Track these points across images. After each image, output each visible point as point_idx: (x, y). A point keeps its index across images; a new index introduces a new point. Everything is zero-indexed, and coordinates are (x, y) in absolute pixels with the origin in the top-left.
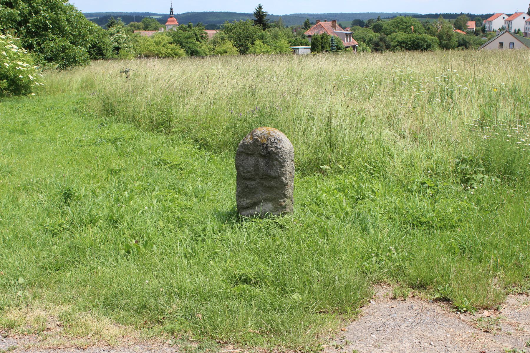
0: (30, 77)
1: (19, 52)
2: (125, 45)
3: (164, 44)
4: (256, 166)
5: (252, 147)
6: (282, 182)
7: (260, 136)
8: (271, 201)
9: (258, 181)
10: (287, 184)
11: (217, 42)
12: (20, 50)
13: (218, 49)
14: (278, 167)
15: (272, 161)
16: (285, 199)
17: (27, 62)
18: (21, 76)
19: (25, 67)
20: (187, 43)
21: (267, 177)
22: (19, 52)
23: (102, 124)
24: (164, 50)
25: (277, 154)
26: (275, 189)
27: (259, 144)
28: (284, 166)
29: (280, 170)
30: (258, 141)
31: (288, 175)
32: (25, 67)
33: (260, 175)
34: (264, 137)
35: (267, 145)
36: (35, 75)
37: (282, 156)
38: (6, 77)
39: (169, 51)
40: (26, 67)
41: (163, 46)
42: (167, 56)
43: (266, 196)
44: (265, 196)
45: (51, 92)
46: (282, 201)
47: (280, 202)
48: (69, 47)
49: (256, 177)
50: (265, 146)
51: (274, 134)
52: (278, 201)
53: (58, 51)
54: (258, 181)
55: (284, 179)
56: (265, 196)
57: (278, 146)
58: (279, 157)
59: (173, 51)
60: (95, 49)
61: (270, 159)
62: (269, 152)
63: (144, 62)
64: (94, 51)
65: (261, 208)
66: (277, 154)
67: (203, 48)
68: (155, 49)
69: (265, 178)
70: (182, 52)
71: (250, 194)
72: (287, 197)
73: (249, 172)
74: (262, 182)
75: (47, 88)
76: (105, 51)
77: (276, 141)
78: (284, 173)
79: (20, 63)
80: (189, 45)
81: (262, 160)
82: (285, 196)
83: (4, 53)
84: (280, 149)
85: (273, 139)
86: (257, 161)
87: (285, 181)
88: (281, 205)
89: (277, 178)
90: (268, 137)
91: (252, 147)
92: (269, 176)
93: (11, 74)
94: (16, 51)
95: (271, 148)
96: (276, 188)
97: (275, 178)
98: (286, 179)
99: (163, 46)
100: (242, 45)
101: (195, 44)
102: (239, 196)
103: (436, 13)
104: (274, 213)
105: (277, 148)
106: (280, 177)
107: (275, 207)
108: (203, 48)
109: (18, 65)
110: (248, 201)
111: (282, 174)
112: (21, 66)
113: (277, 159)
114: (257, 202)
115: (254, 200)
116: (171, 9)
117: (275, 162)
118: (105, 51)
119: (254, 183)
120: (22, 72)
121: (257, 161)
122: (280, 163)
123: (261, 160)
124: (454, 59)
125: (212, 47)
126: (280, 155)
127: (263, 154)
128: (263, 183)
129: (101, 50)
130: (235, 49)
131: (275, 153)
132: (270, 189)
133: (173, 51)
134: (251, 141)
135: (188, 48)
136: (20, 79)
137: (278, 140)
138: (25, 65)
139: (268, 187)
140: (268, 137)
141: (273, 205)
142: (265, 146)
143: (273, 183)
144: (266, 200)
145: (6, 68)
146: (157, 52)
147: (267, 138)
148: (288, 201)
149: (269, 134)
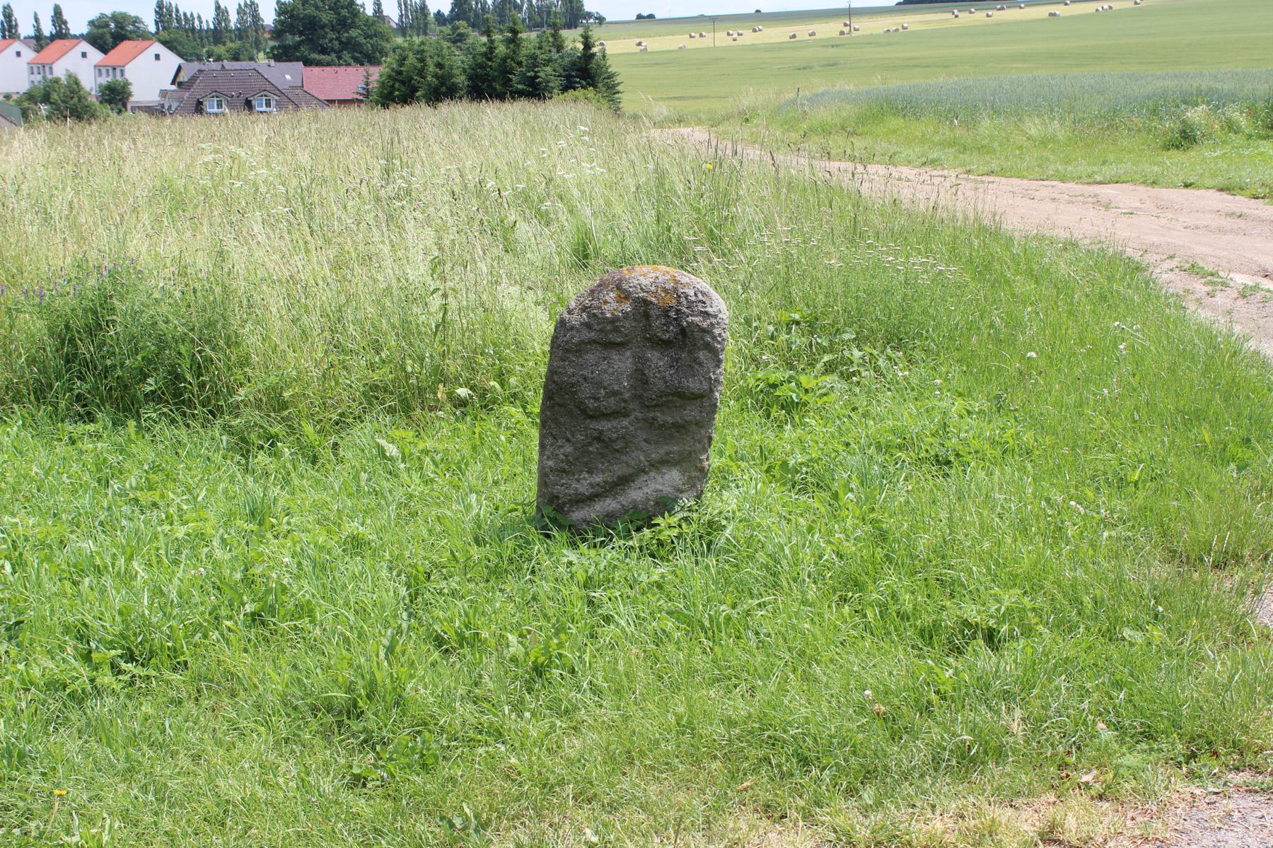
4: (641, 378)
7: (653, 289)
34: (665, 290)
35: (678, 312)
43: (662, 451)
44: (657, 453)
50: (672, 314)
56: (657, 453)
57: (709, 309)
58: (714, 338)
62: (683, 331)
73: (615, 394)
74: (651, 415)
77: (700, 297)
81: (657, 354)
84: (716, 317)
85: (692, 293)
95: (690, 319)
96: (697, 424)
103: (123, 10)
107: (690, 477)
110: (598, 478)
114: (631, 475)
115: (620, 470)
116: (37, 20)
119: (625, 422)
121: (640, 360)
123: (653, 356)
124: (498, 120)
126: (717, 331)
131: (704, 331)
134: (627, 307)
140: (675, 289)
141: (683, 472)
142: (672, 314)
149: (677, 282)
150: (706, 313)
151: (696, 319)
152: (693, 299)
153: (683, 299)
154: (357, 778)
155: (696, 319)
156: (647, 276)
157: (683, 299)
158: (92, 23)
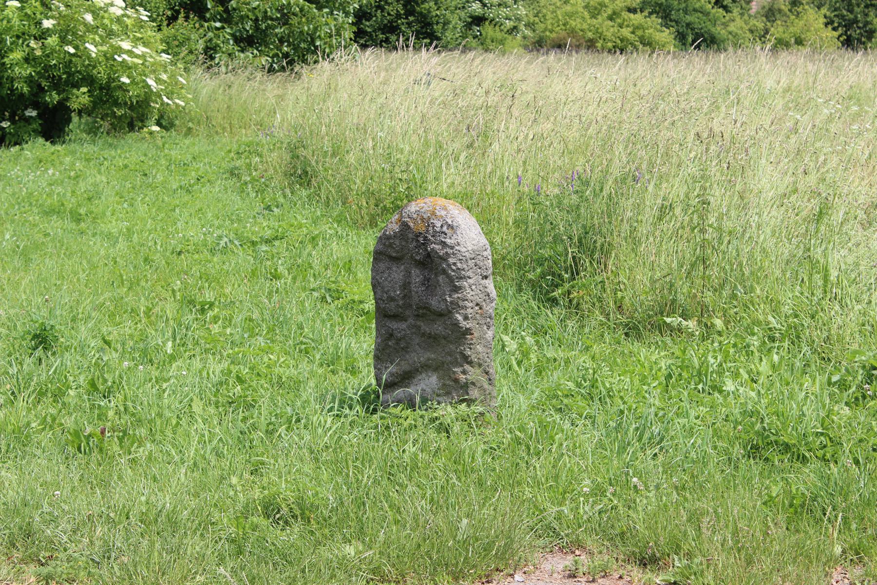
0: (151, 82)
1: (129, 17)
2: (503, 12)
3: (614, 13)
5: (397, 242)
6: (456, 324)
7: (415, 216)
8: (436, 369)
9: (411, 321)
10: (468, 331)
11: (780, 11)
12: (130, 12)
13: (777, 30)
14: (447, 289)
15: (436, 275)
16: (467, 367)
17: (145, 44)
18: (125, 80)
19: (137, 56)
20: (686, 12)
21: (426, 313)
22: (129, 17)
23: (268, 208)
24: (610, 30)
25: (444, 258)
26: (443, 341)
27: (410, 236)
28: (460, 288)
29: (450, 296)
30: (409, 227)
31: (469, 311)
32: (137, 56)
33: (417, 311)
34: (422, 219)
35: (425, 238)
36: (164, 77)
37: (454, 264)
38: (90, 81)
39: (626, 32)
40: (143, 56)
41: (611, 18)
42: (621, 48)
43: (426, 356)
45: (224, 129)
46: (458, 370)
47: (454, 372)
48: (302, 10)
49: (407, 313)
50: (421, 240)
51: (443, 213)
52: (449, 369)
53: (272, 19)
54: (411, 321)
55: (460, 318)
57: (448, 241)
58: (449, 265)
59: (639, 33)
60: (411, 18)
61: (431, 270)
62: (429, 255)
63: (481, 58)
64: (409, 25)
65: (415, 390)
66: (444, 258)
67: (732, 27)
68: (585, 26)
69: (423, 316)
70: (666, 36)
71: (398, 352)
72: (470, 363)
73: (392, 299)
75: (218, 119)
76: (440, 26)
77: (445, 229)
78: (461, 303)
79: (126, 45)
80: (689, 18)
81: (418, 271)
82: (467, 360)
83: (89, 18)
84: (452, 248)
85: (439, 224)
86: (408, 274)
87: (464, 324)
88: (456, 381)
89: (445, 314)
90: (429, 218)
91: (397, 242)
92: (429, 310)
93: (101, 73)
94: (120, 12)
97: (441, 315)
98: (466, 318)
99: (611, 18)
100: (856, 21)
101: (707, 14)
102: (381, 356)
104: (440, 399)
105: (444, 244)
106: (450, 312)
107: (444, 385)
108: (732, 27)
109: (119, 50)
111: (457, 306)
112: (130, 53)
113: (444, 272)
114: (410, 372)
115: (405, 367)
117: (441, 278)
118: (440, 26)
120: (130, 68)
121: (408, 274)
122: (451, 280)
125: (760, 25)
127: (418, 258)
128: (420, 327)
129: (430, 24)
130: (830, 33)
131: (441, 258)
132: (432, 340)
133: (639, 33)
135: (688, 25)
136: (122, 87)
137: (450, 227)
138: (140, 50)
139: (430, 336)
141: (439, 378)
142: (421, 240)
143: (438, 328)
144: (426, 367)
145: (89, 58)
146: (590, 35)
147: (427, 222)
148: (473, 374)
150: (444, 243)
151: (437, 247)
152: (438, 229)
153: (431, 228)
154: (207, 49)
155: (437, 247)
156: (58, 147)
157: (431, 228)
158: (299, 76)
